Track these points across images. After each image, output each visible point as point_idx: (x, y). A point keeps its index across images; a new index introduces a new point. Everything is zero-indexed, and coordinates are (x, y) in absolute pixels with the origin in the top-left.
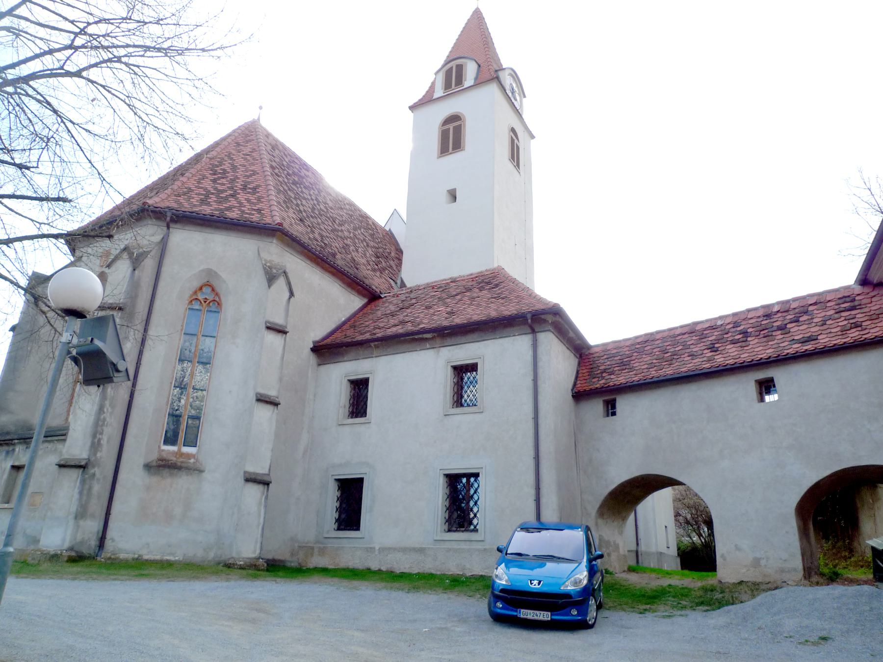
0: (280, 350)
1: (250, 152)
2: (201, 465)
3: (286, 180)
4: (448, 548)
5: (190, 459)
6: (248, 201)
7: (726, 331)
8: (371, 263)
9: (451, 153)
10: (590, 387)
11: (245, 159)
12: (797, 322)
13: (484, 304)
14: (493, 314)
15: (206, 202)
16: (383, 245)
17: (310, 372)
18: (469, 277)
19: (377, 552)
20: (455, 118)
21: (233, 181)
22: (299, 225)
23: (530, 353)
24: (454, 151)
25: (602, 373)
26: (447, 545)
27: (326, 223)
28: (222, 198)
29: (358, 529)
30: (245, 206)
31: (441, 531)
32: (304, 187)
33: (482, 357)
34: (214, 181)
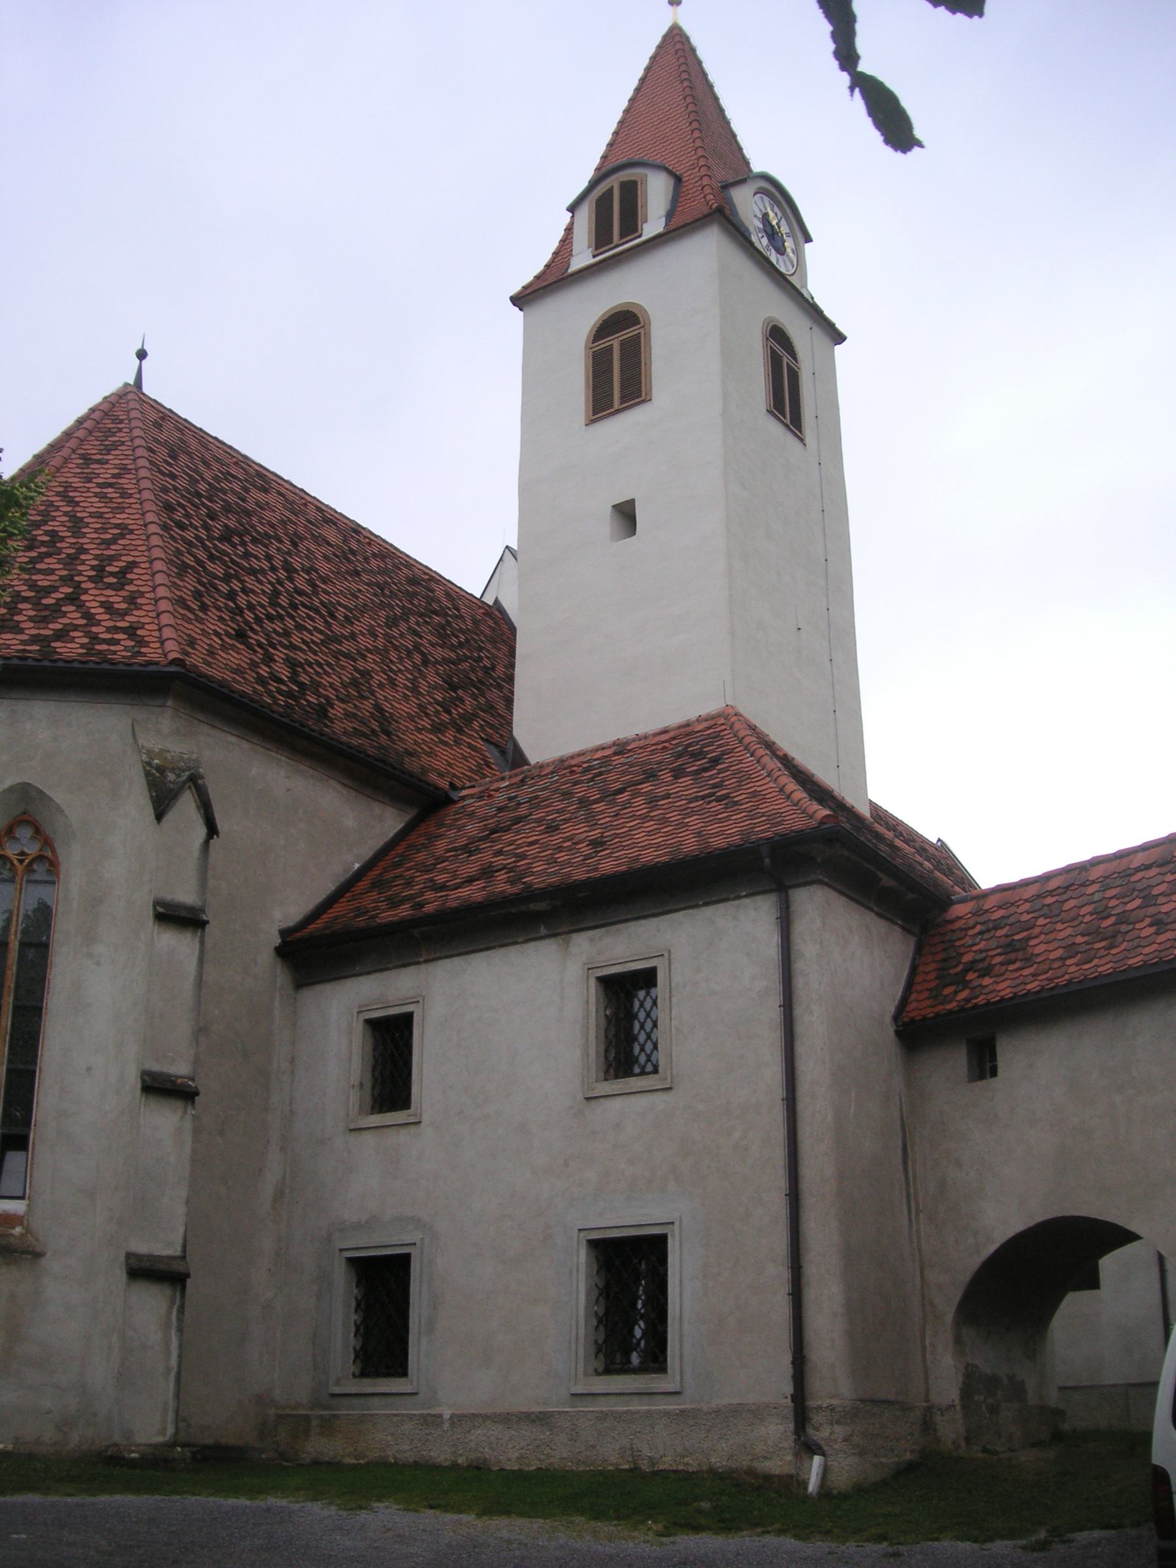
0: (191, 966)
1: (114, 476)
2: (37, 1240)
4: (602, 1412)
5: (13, 1228)
6: (108, 607)
8: (431, 710)
9: (618, 411)
10: (936, 1010)
11: (102, 497)
13: (674, 816)
14: (690, 844)
15: (11, 624)
16: (470, 651)
17: (277, 1004)
19: (446, 1426)
21: (72, 560)
22: (233, 647)
23: (775, 939)
25: (966, 971)
26: (601, 1406)
27: (309, 625)
28: (47, 607)
29: (404, 1373)
30: (98, 623)
31: (586, 1374)
33: (666, 954)
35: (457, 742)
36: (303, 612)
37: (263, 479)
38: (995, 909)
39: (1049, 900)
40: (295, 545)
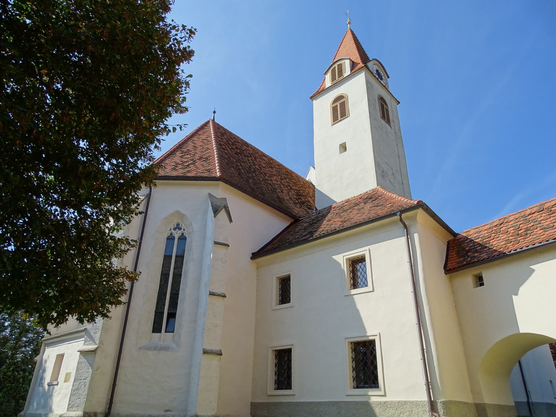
9: (340, 121)
18: (357, 197)
20: (340, 97)
32: (244, 156)
34: (182, 157)
35: (300, 207)
36: (257, 173)
38: (474, 234)
40: (255, 159)
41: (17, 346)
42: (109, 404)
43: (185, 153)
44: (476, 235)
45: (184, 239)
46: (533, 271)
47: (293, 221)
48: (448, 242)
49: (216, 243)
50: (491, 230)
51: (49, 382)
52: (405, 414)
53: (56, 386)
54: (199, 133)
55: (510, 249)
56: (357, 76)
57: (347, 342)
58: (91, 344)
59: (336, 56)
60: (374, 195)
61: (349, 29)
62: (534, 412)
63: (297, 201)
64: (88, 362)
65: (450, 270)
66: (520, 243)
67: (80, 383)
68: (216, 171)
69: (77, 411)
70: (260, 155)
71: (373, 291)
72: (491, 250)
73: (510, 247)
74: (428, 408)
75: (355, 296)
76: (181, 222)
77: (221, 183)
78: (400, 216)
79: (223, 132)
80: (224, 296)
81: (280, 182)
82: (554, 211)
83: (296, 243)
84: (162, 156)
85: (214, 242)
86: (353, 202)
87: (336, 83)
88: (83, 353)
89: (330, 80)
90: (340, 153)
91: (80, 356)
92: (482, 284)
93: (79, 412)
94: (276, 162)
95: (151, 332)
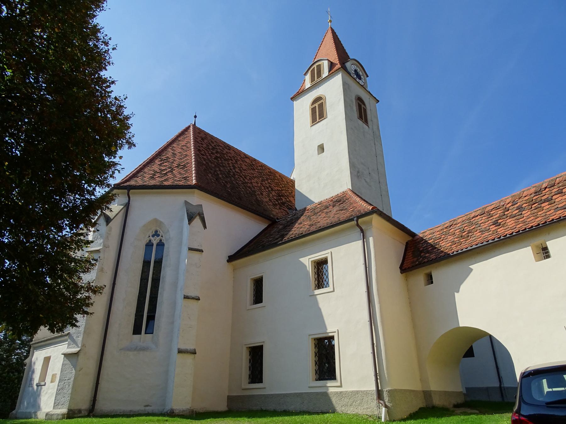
3: (209, 157)
7: (507, 209)
9: (318, 122)
12: (561, 193)
18: (329, 200)
20: (319, 99)
24: (320, 120)
34: (160, 165)
35: (280, 209)
37: (229, 147)
39: (445, 230)
40: (236, 162)
41: (11, 348)
42: (92, 401)
43: (164, 160)
44: (431, 236)
45: (162, 245)
46: (472, 270)
47: (270, 223)
48: (407, 243)
49: (190, 249)
50: (442, 232)
51: (37, 382)
52: (357, 403)
53: (43, 387)
54: (179, 139)
55: (453, 250)
56: (335, 78)
57: (311, 339)
58: (74, 347)
59: (316, 56)
60: (343, 198)
61: (329, 27)
62: (506, 396)
63: (277, 203)
64: (71, 364)
65: (405, 269)
66: (462, 245)
67: (64, 383)
68: (192, 179)
69: (62, 408)
70: (241, 157)
71: (334, 291)
72: (439, 251)
73: (454, 248)
74: (375, 397)
75: (318, 296)
76: (160, 230)
77: (196, 191)
78: (357, 221)
79: (204, 136)
80: (198, 299)
81: (261, 184)
82: (492, 215)
83: (268, 246)
84: (131, 173)
85: (189, 248)
86: (324, 204)
87: (315, 84)
88: (66, 355)
89: (309, 81)
90: (318, 154)
91: (64, 359)
92: (548, 256)
93: (64, 410)
94: (259, 162)
95: (132, 334)
